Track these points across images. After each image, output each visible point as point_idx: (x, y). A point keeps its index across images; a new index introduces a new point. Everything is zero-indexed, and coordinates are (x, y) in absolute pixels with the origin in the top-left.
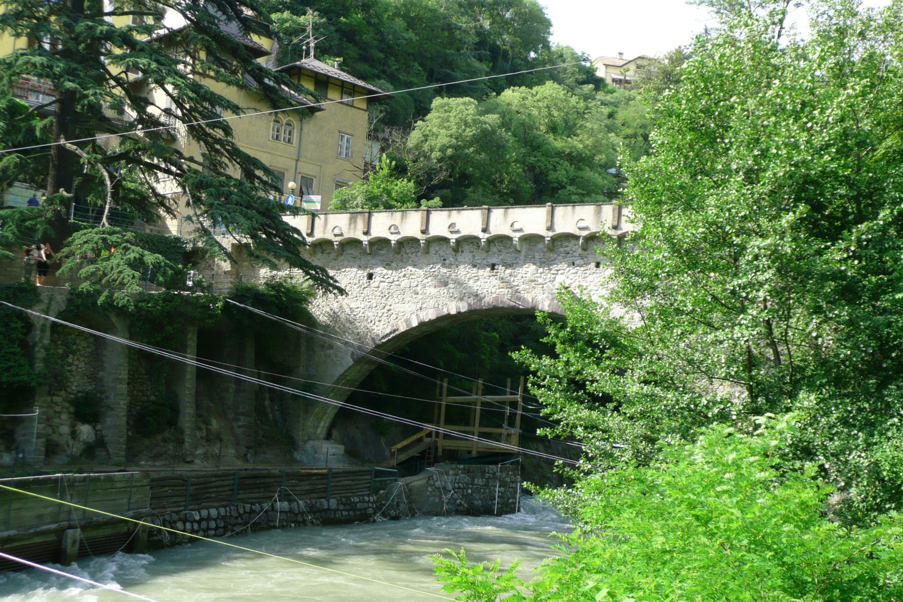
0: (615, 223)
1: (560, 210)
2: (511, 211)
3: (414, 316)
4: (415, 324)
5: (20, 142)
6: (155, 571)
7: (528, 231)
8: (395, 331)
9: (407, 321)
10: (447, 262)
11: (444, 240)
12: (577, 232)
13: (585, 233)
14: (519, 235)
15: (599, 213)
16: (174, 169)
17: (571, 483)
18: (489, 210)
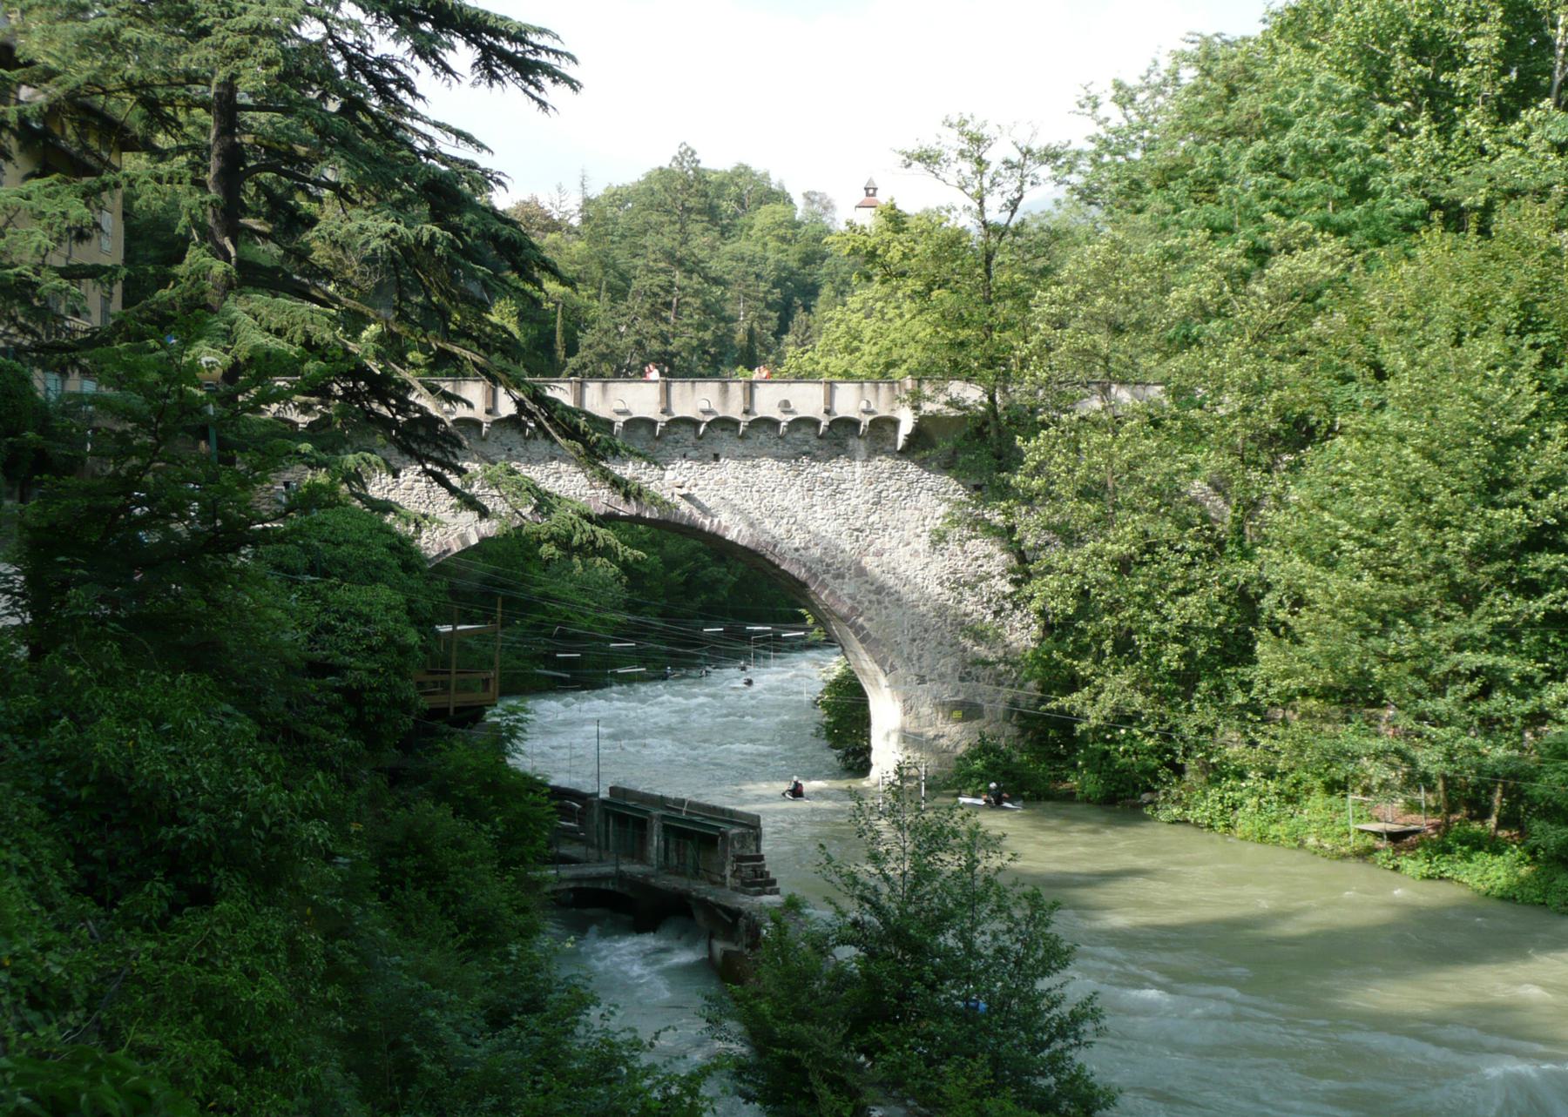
0: (490, 406)
1: (677, 388)
2: (610, 385)
3: (471, 530)
4: (474, 540)
5: (779, 318)
6: (1111, 824)
7: (638, 413)
8: (445, 552)
9: (462, 537)
10: (514, 452)
11: (772, 423)
12: (700, 417)
13: (709, 418)
14: (623, 418)
15: (725, 391)
16: (488, 329)
17: (407, 932)
18: (581, 383)
